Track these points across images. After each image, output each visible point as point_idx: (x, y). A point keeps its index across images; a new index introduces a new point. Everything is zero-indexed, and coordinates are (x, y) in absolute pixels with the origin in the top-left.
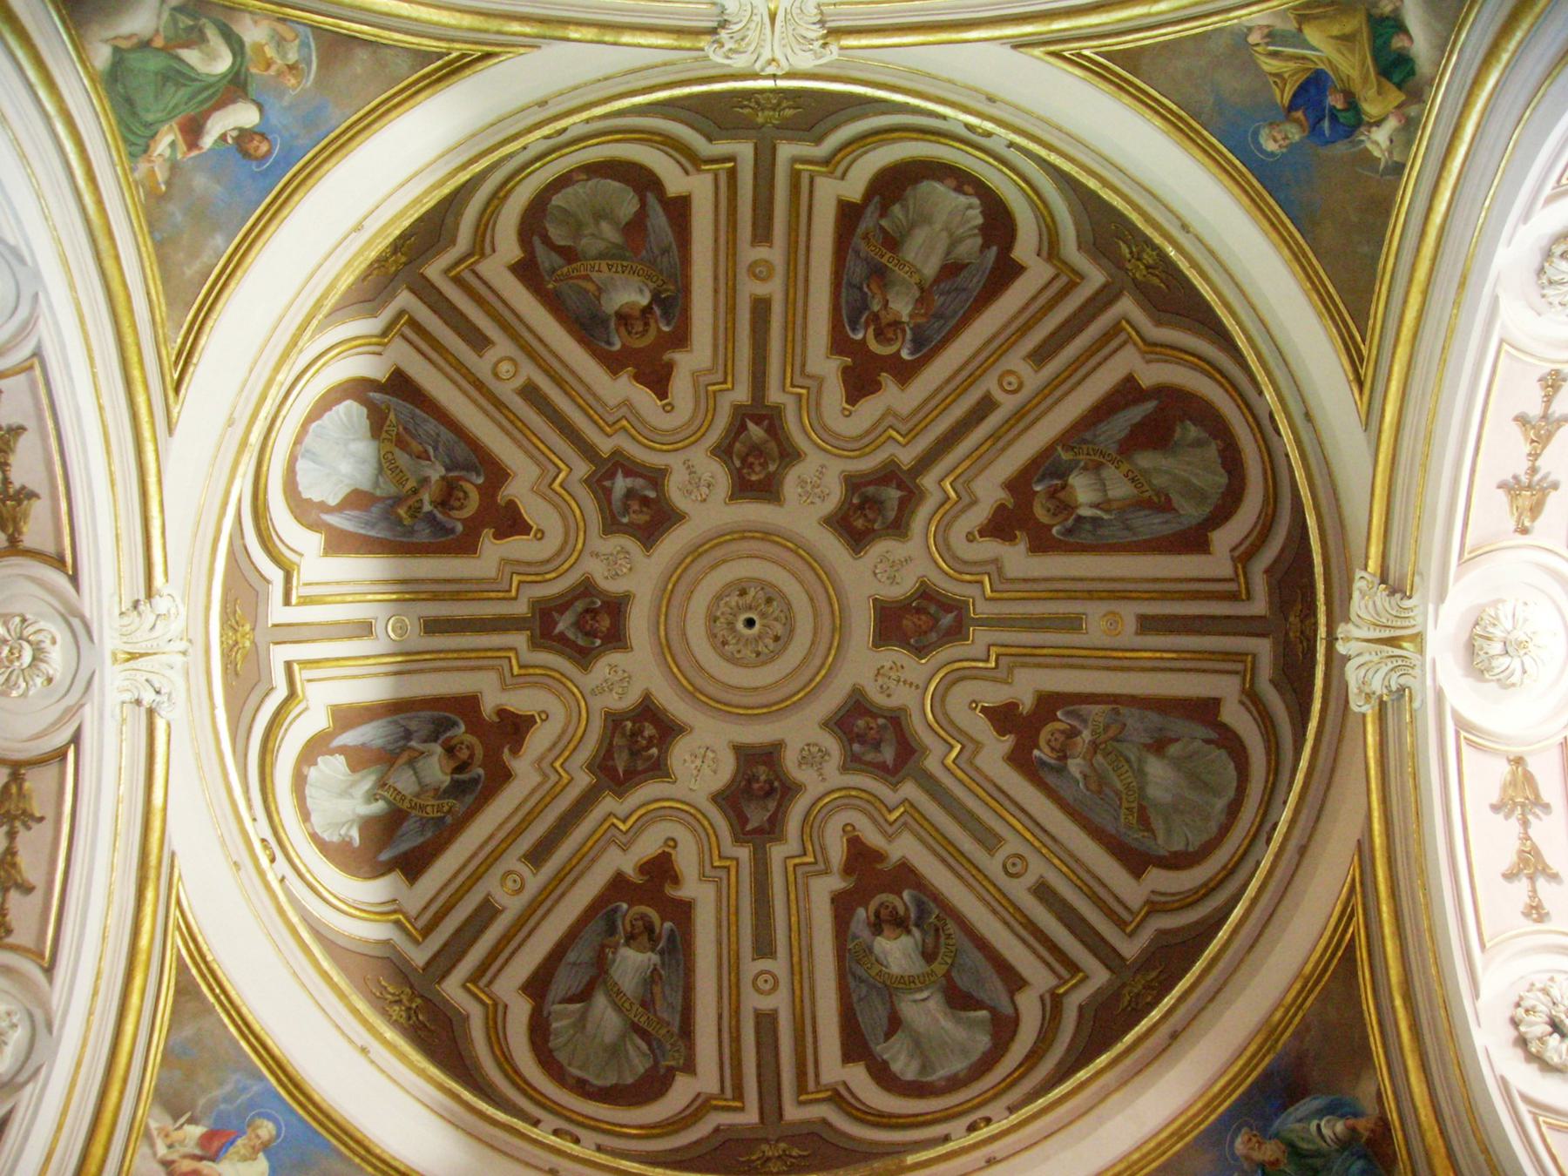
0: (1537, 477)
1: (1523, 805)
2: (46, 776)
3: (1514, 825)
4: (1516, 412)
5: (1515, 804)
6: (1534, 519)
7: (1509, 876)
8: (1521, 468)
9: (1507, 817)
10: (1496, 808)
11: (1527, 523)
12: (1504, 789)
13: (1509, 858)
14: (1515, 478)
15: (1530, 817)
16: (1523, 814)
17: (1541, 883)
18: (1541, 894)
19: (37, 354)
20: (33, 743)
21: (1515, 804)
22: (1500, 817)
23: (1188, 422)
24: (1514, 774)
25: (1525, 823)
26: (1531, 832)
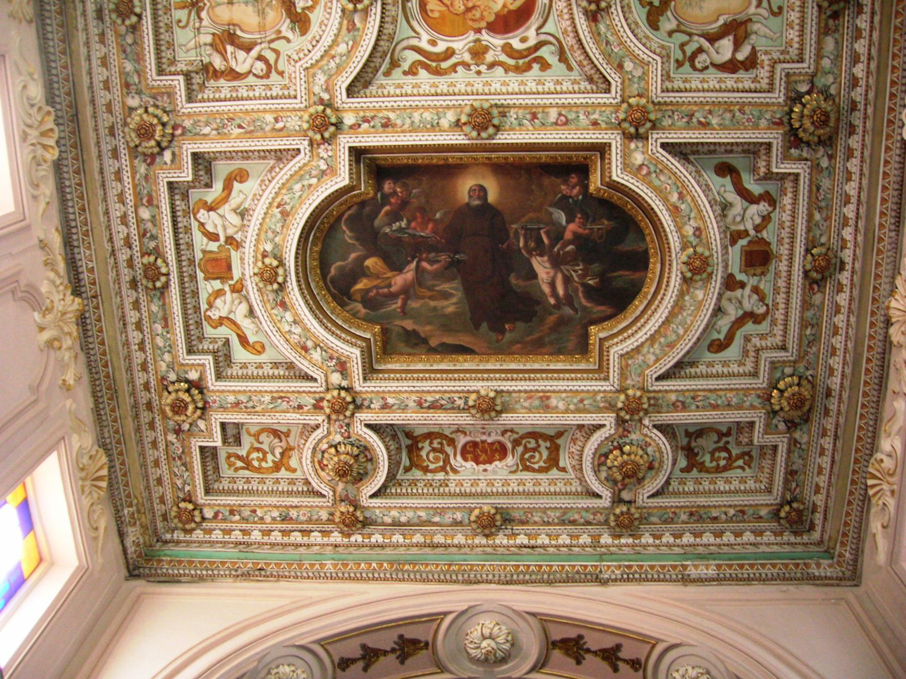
0: (397, 647)
1: (578, 648)
2: (552, 628)
3: (588, 656)
4: (363, 673)
5: (577, 652)
6: (419, 641)
7: (616, 669)
8: (392, 657)
9: (584, 659)
10: (579, 663)
11: (422, 644)
12: (568, 655)
13: (605, 666)
14: (398, 658)
15: (585, 647)
16: (583, 650)
17: (621, 655)
18: (627, 657)
19: (318, 642)
20: (535, 629)
21: (577, 652)
22: (584, 662)
23: (353, 290)
24: (560, 648)
25: (588, 651)
26: (593, 649)
